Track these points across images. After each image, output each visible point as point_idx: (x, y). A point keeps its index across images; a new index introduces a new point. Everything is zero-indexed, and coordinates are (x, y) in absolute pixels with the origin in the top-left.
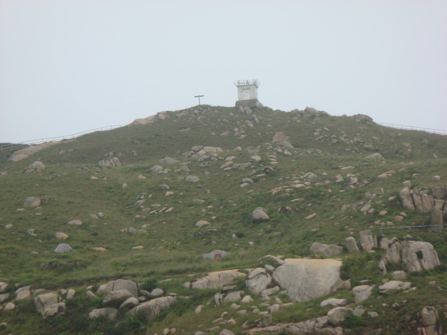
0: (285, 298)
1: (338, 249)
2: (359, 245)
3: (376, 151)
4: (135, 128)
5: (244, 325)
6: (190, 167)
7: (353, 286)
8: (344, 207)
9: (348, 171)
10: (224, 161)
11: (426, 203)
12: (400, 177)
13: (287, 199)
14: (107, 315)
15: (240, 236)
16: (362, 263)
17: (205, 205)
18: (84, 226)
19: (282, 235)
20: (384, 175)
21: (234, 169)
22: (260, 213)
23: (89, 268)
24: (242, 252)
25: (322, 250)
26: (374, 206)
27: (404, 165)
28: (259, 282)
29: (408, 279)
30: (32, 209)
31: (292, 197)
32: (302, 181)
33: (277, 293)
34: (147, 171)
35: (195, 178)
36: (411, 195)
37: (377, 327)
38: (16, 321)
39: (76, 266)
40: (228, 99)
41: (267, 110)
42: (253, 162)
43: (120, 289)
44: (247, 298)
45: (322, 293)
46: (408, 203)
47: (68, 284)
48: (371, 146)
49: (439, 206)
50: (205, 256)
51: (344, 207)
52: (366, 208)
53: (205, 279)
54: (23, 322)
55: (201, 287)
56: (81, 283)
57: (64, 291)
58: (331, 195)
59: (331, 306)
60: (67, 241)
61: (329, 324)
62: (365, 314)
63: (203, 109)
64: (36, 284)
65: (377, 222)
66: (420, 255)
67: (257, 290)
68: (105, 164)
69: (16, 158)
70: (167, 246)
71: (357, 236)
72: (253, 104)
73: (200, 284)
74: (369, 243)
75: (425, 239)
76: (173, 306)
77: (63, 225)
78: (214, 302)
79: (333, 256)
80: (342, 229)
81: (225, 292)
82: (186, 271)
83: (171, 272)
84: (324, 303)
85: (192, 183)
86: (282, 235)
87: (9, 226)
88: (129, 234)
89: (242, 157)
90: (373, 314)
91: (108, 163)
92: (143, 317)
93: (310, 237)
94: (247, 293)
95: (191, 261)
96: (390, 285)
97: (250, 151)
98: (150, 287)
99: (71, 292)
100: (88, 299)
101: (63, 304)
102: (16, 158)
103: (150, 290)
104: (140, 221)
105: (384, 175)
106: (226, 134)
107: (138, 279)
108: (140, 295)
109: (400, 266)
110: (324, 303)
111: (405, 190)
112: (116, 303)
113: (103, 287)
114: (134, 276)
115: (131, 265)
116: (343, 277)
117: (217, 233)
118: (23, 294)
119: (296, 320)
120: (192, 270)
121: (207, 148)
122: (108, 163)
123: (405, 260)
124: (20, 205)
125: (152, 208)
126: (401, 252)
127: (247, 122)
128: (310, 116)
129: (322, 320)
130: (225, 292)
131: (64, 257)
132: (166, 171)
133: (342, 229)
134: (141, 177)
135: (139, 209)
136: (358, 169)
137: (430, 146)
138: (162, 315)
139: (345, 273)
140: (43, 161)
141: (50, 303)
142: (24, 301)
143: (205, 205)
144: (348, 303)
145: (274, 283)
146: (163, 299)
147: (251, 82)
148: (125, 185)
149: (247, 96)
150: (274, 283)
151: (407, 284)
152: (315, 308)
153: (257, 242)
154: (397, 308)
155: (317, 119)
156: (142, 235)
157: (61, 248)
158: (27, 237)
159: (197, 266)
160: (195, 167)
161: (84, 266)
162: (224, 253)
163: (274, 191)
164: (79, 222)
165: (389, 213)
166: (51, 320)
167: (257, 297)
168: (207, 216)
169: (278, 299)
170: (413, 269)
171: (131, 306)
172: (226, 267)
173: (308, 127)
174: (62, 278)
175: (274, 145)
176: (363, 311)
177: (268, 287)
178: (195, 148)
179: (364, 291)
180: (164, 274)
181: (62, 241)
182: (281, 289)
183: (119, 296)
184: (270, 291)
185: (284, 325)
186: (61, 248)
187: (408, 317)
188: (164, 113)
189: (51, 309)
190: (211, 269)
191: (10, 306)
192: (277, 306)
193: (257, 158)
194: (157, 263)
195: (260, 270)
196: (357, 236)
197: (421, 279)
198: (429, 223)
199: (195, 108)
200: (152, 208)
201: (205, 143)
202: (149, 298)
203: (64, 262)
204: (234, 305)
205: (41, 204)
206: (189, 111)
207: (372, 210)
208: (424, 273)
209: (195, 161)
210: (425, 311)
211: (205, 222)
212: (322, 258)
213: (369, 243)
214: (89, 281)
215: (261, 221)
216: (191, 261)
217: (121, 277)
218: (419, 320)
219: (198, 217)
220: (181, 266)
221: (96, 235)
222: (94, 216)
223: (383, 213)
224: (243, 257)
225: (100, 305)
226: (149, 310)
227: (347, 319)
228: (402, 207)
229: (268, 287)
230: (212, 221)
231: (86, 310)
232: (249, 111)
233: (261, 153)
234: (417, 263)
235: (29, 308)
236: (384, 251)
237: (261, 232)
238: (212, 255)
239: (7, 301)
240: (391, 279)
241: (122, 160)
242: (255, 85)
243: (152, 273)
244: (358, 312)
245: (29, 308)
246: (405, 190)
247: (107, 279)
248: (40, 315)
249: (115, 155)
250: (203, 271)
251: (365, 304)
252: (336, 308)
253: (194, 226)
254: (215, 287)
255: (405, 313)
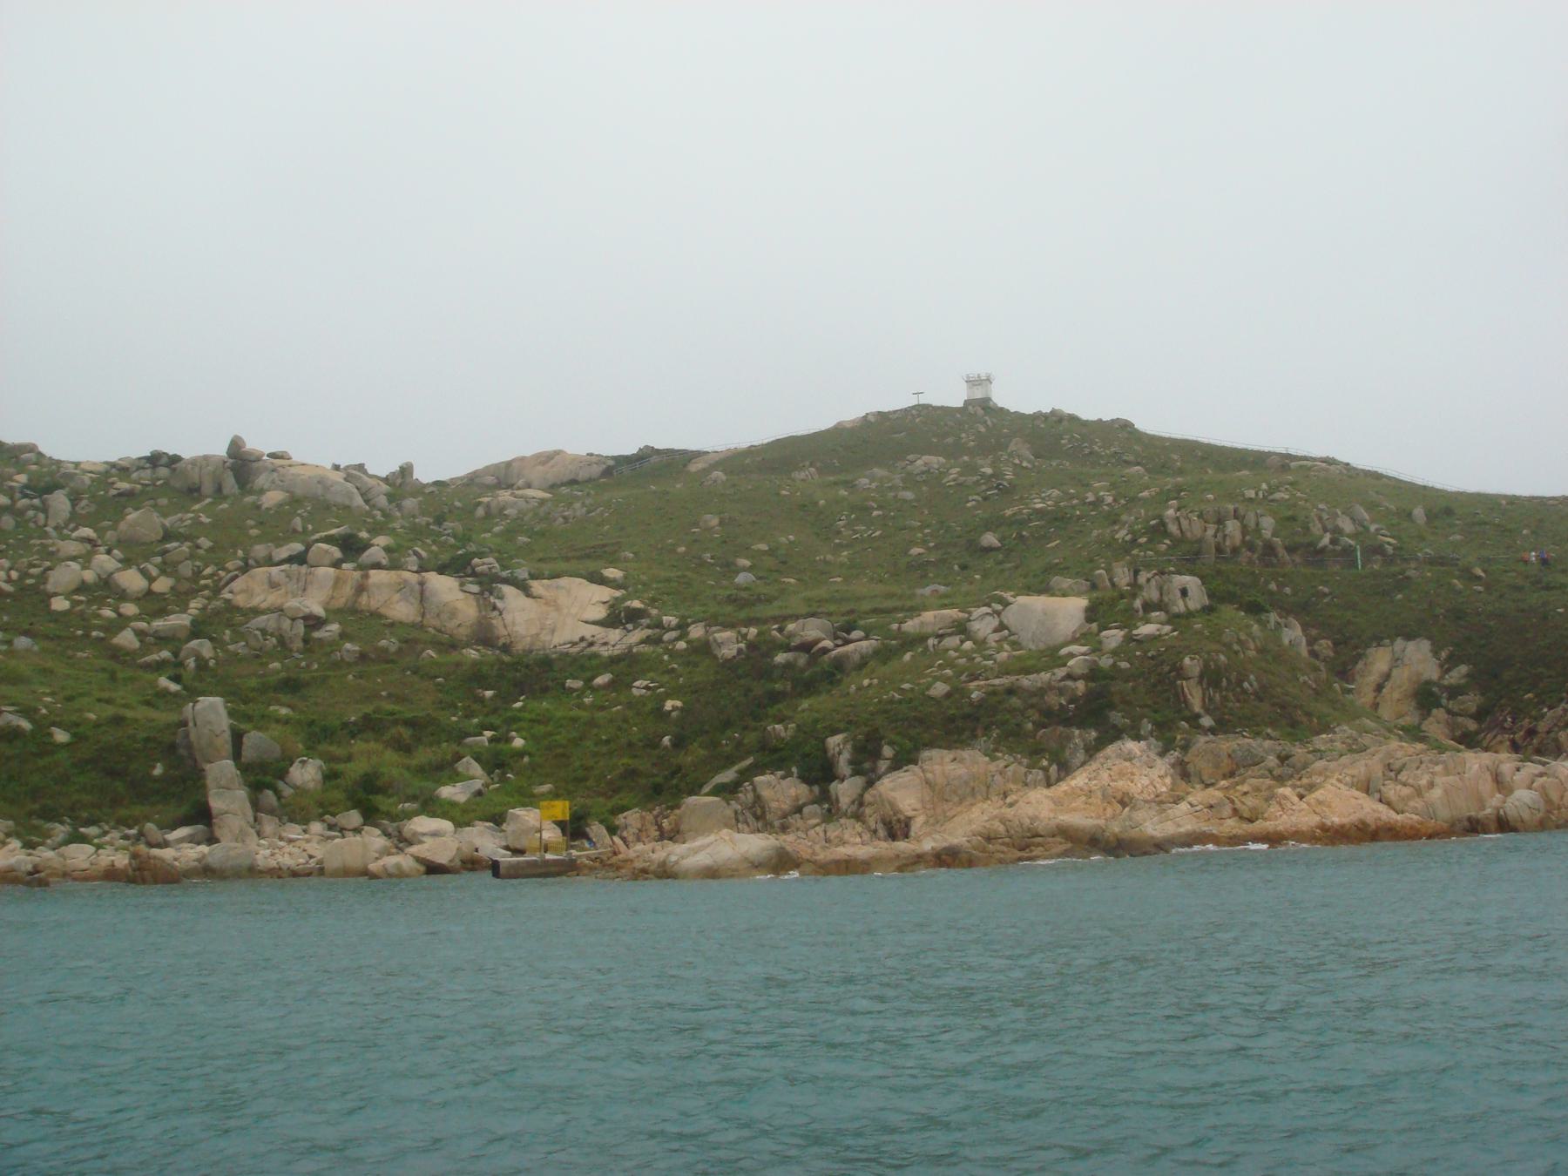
0: (1016, 645)
1: (1085, 585)
2: (1111, 580)
3: (1138, 464)
4: (838, 431)
5: (963, 678)
6: (903, 480)
7: (1100, 631)
8: (1095, 533)
9: (1102, 488)
10: (946, 473)
11: (1194, 528)
12: (1164, 498)
13: (1023, 523)
14: (796, 660)
15: (964, 567)
16: (1113, 603)
17: (921, 528)
18: (771, 552)
19: (1017, 568)
20: (1145, 494)
21: (960, 485)
22: (990, 539)
23: (776, 604)
24: (965, 588)
25: (1065, 586)
26: (1130, 532)
27: (1170, 482)
28: (983, 626)
29: (1168, 623)
30: (709, 529)
31: (1030, 520)
32: (1043, 500)
33: (1005, 638)
34: (849, 485)
35: (909, 495)
36: (1178, 519)
37: (1127, 681)
38: (688, 664)
39: (759, 600)
40: (954, 396)
41: (1002, 411)
42: (983, 475)
43: (812, 630)
44: (968, 645)
45: (1061, 640)
46: (1173, 528)
47: (749, 622)
48: (1131, 458)
49: (1210, 532)
50: (919, 591)
51: (1095, 533)
52: (1122, 534)
53: (916, 621)
54: (696, 665)
55: (911, 630)
56: (765, 621)
57: (744, 630)
58: (1079, 518)
59: (1071, 655)
60: (749, 569)
61: (1069, 677)
62: (1114, 665)
63: (924, 410)
64: (712, 621)
65: (1135, 552)
66: (1184, 592)
67: (981, 635)
68: (799, 475)
69: (694, 467)
70: (872, 579)
71: (1109, 570)
72: (985, 405)
73: (911, 626)
74: (1123, 577)
75: (1192, 573)
76: (876, 653)
77: (745, 550)
78: (926, 648)
79: (1079, 594)
80: (1091, 561)
81: (941, 637)
82: (895, 610)
83: (875, 611)
84: (1064, 651)
85: (905, 501)
86: (1017, 568)
87: (682, 549)
88: (826, 562)
89: (970, 469)
90: (1124, 665)
91: (803, 475)
92: (839, 665)
93: (1051, 569)
94: (968, 639)
95: (901, 597)
96: (1146, 629)
97: (980, 462)
98: (849, 629)
99: (753, 631)
100: (774, 640)
101: (742, 645)
102: (694, 467)
103: (848, 633)
104: (840, 546)
105: (1145, 494)
106: (950, 440)
107: (834, 618)
108: (836, 637)
109: (1160, 606)
110: (1064, 651)
111: (1171, 512)
112: (806, 647)
113: (791, 627)
114: (830, 614)
115: (827, 601)
116: (1089, 620)
117: (934, 564)
118: (696, 632)
119: (1027, 671)
120: (902, 609)
121: (926, 458)
122: (803, 475)
123: (1166, 599)
124: (696, 524)
125: (855, 532)
126: (1161, 589)
127: (977, 428)
128: (1057, 420)
129: (1061, 672)
130: (941, 637)
131: (746, 589)
132: (874, 485)
133: (1091, 561)
134: (843, 492)
135: (839, 532)
136: (1113, 486)
137: (1203, 459)
138: (863, 664)
139: (1091, 614)
140: (724, 471)
141: (728, 643)
142: (698, 639)
143: (921, 528)
144: (1093, 651)
145: (1002, 627)
146: (864, 643)
147: (218, 833)
148: (822, 502)
149: (978, 394)
150: (1002, 627)
151: (1167, 628)
152: (1052, 656)
153: (985, 576)
154: (1153, 658)
155: (1065, 423)
156: (842, 565)
157: (742, 578)
158: (703, 564)
159: (909, 603)
160: (910, 481)
161: (770, 600)
162: (942, 588)
163: (1008, 512)
164: (764, 547)
165: (1150, 541)
166: (729, 664)
167: (981, 644)
168: (924, 543)
169: (1006, 647)
170: (1175, 610)
171: (825, 651)
172: (945, 606)
173: (1055, 435)
174: (743, 615)
175: (1011, 455)
176: (1111, 661)
177: (996, 631)
178: (911, 457)
179: (1113, 637)
180: (866, 613)
181: (744, 569)
182: (1011, 634)
183: (810, 639)
184: (997, 636)
185: (1013, 678)
186: (742, 578)
187: (1167, 668)
188: (873, 414)
189: (728, 651)
190: (926, 609)
191: (682, 645)
192: (1005, 654)
193: (989, 471)
194: (859, 599)
195: (985, 610)
196: (1109, 570)
197: (1183, 622)
198: (1198, 553)
199: (913, 407)
200: (855, 532)
201: (924, 452)
202: (847, 642)
203: (744, 594)
204: (952, 653)
205: (721, 523)
206: (906, 411)
207: (1128, 538)
208: (1189, 615)
209: (909, 474)
210: (1187, 660)
211: (921, 550)
212: (1064, 596)
213: (1123, 577)
214: (775, 619)
215: (990, 549)
216: (901, 597)
217: (813, 615)
218: (1179, 672)
219: (913, 543)
220: (889, 604)
221: (784, 563)
222: (783, 539)
223: (1143, 540)
224: (967, 594)
225: (788, 649)
226: (846, 656)
227: (1092, 670)
228: (1166, 534)
229: (996, 631)
230: (928, 549)
231: (770, 654)
232: (981, 412)
233: (992, 465)
234: (1181, 603)
235: (704, 649)
236: (1141, 588)
237: (990, 564)
238: (927, 591)
239: (678, 639)
240: (1148, 622)
241: (820, 471)
242: (989, 380)
243: (852, 612)
244: (1105, 662)
245: (704, 649)
246: (1171, 512)
247: (796, 617)
248: (715, 657)
249: (811, 465)
250: (914, 611)
251: (1115, 653)
252: (1078, 657)
253: (906, 553)
254: (929, 630)
255: (1162, 663)
